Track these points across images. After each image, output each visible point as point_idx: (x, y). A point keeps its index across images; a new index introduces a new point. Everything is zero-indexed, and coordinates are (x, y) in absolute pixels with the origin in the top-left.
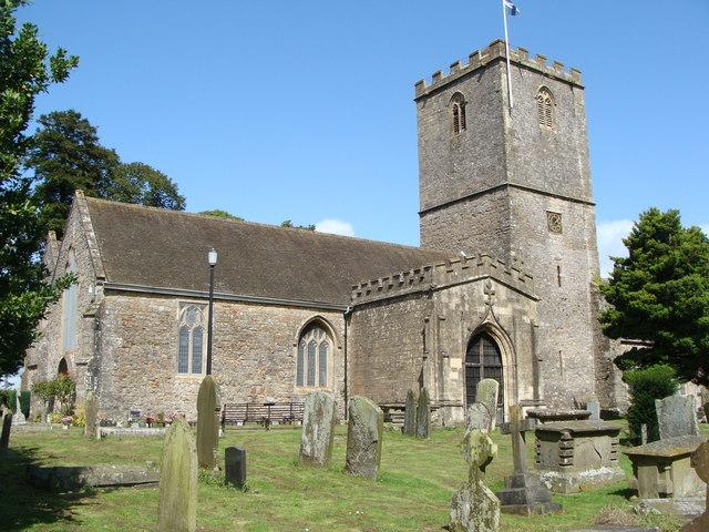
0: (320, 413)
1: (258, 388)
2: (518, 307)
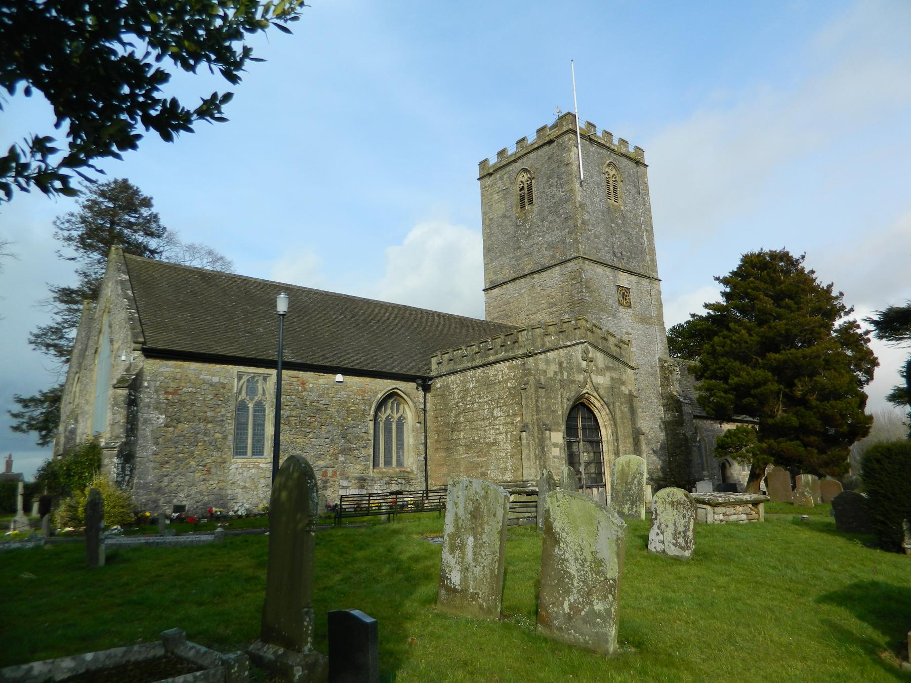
0: (475, 515)
1: (330, 471)
2: (615, 375)
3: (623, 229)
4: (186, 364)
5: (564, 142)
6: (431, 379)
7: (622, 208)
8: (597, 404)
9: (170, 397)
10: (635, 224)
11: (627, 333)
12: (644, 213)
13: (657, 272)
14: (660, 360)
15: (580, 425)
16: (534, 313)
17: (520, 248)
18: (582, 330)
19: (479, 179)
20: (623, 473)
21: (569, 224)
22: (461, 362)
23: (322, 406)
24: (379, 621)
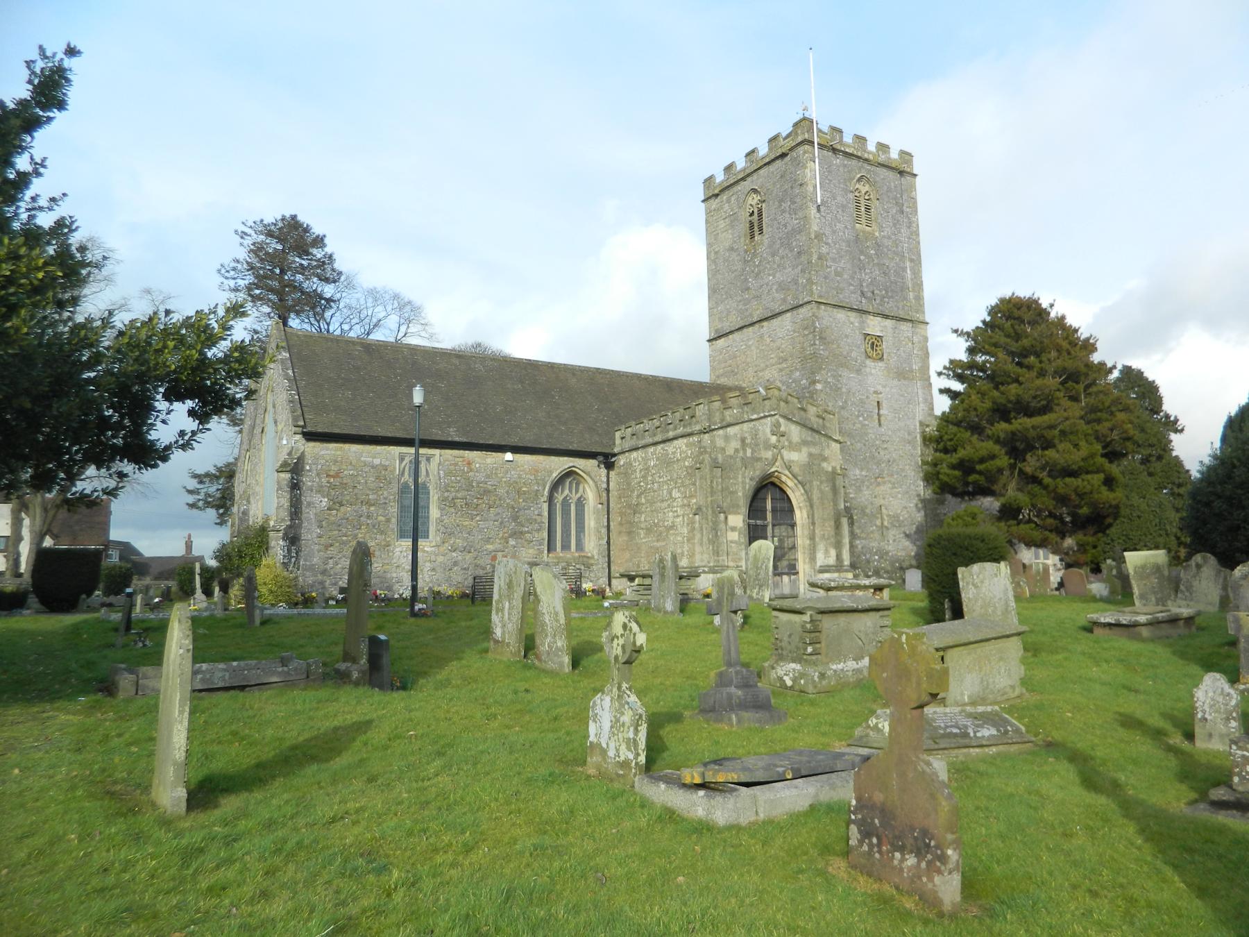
0: (510, 585)
2: (813, 450)
3: (876, 261)
4: (347, 446)
5: (798, 156)
6: (615, 455)
7: (877, 234)
8: (790, 483)
9: (332, 480)
10: (895, 253)
11: (876, 392)
12: (909, 238)
13: (923, 313)
14: (921, 424)
15: (769, 506)
16: (763, 370)
17: (748, 289)
18: (774, 401)
19: (703, 201)
20: (756, 558)
21: (802, 259)
22: (643, 437)
23: (490, 487)
24: (392, 642)
